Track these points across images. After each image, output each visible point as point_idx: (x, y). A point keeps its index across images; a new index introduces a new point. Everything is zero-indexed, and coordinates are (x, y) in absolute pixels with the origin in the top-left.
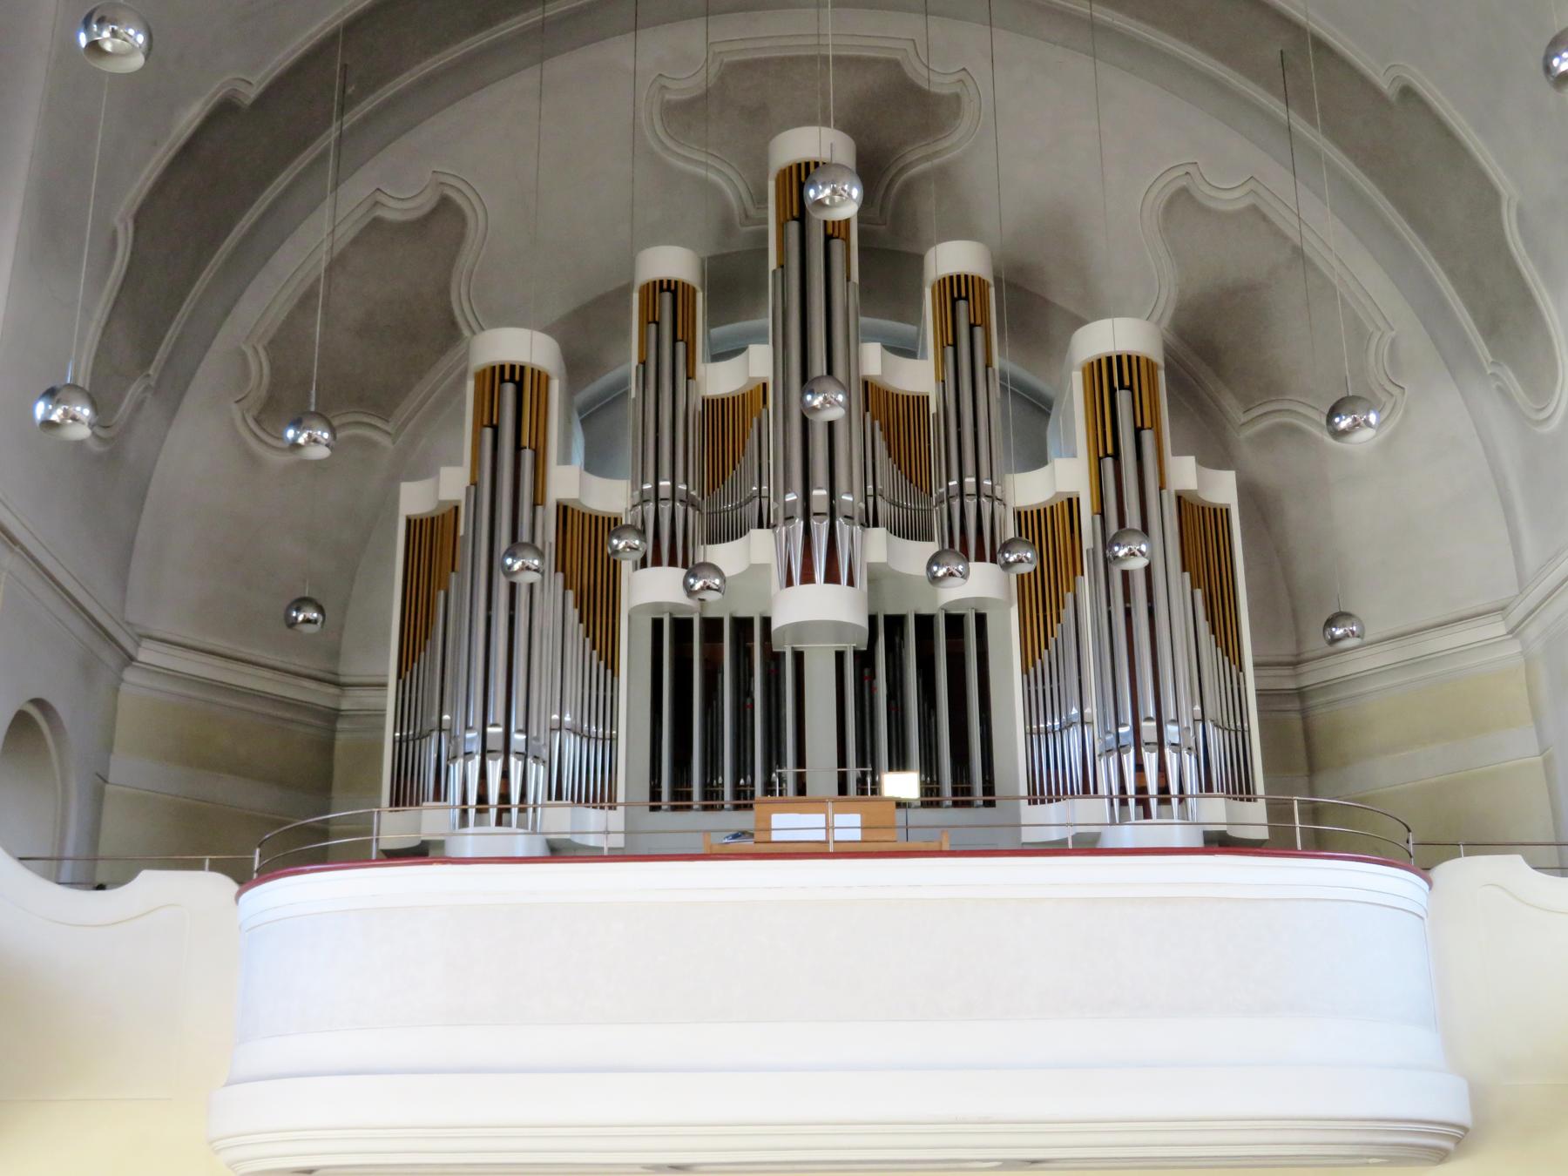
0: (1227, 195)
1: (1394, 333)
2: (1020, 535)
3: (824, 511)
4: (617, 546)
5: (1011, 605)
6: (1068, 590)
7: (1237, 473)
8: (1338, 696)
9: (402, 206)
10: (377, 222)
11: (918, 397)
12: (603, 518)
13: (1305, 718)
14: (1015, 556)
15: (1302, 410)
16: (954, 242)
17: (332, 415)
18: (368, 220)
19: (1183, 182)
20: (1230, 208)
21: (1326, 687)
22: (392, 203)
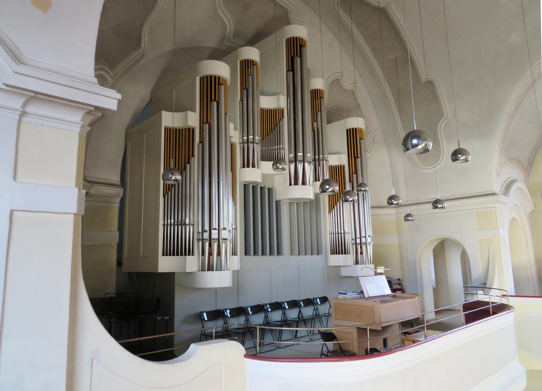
0: (348, 85)
1: (375, 133)
2: (330, 178)
6: (338, 201)
11: (267, 110)
14: (364, 189)
16: (225, 64)
17: (423, 78)
19: (339, 77)
20: (347, 88)
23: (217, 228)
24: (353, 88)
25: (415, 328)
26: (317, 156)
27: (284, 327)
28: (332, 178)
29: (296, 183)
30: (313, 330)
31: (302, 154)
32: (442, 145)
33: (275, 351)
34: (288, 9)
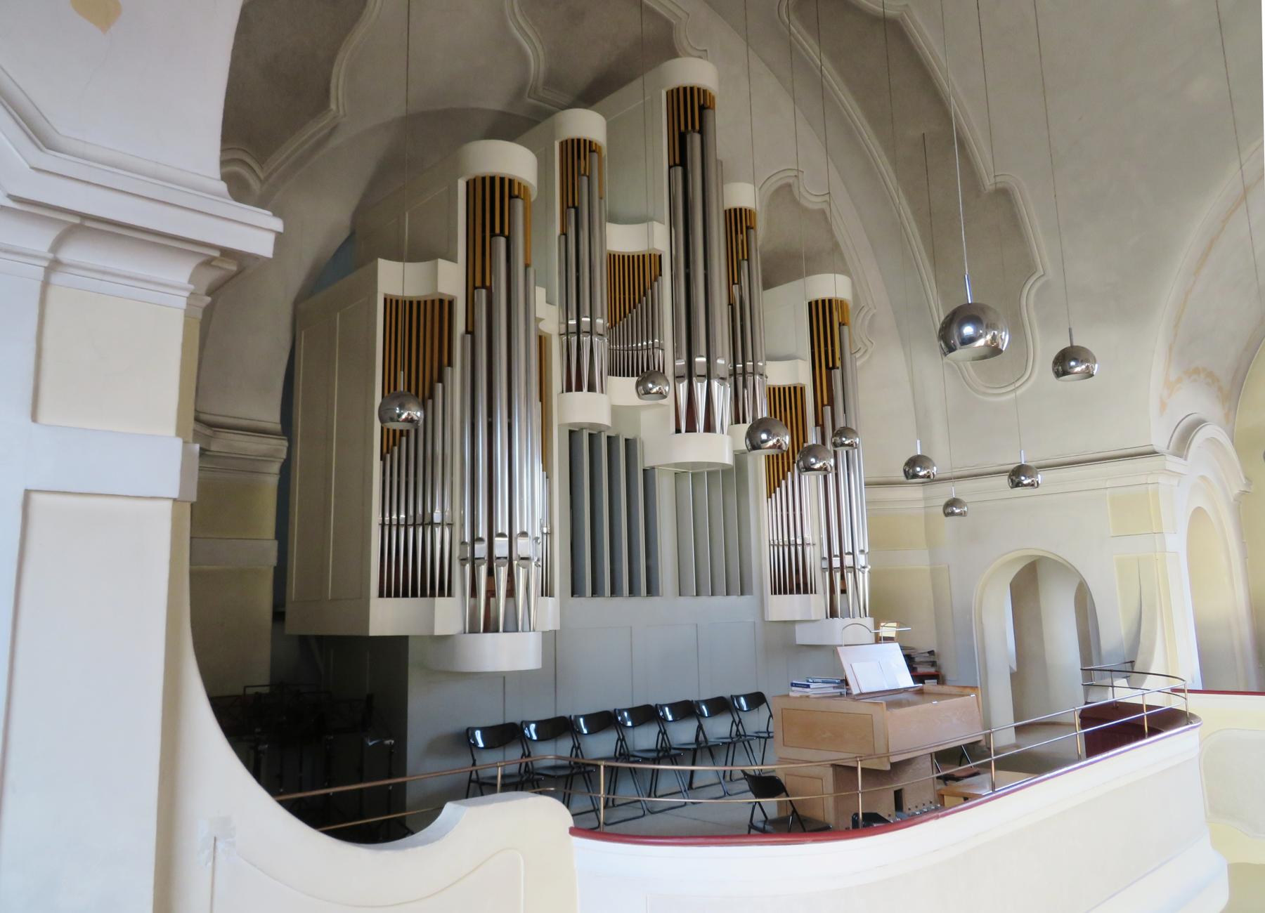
0: (811, 198)
1: (875, 311)
4: (651, 389)
6: (789, 470)
7: (268, 259)
11: (623, 257)
12: (619, 256)
14: (850, 441)
16: (526, 149)
19: (791, 181)
20: (810, 206)
23: (507, 533)
24: (824, 206)
25: (969, 765)
26: (739, 364)
27: (663, 765)
28: (776, 417)
29: (691, 428)
30: (731, 771)
31: (704, 359)
32: (1032, 337)
33: (643, 819)
34: (673, 21)
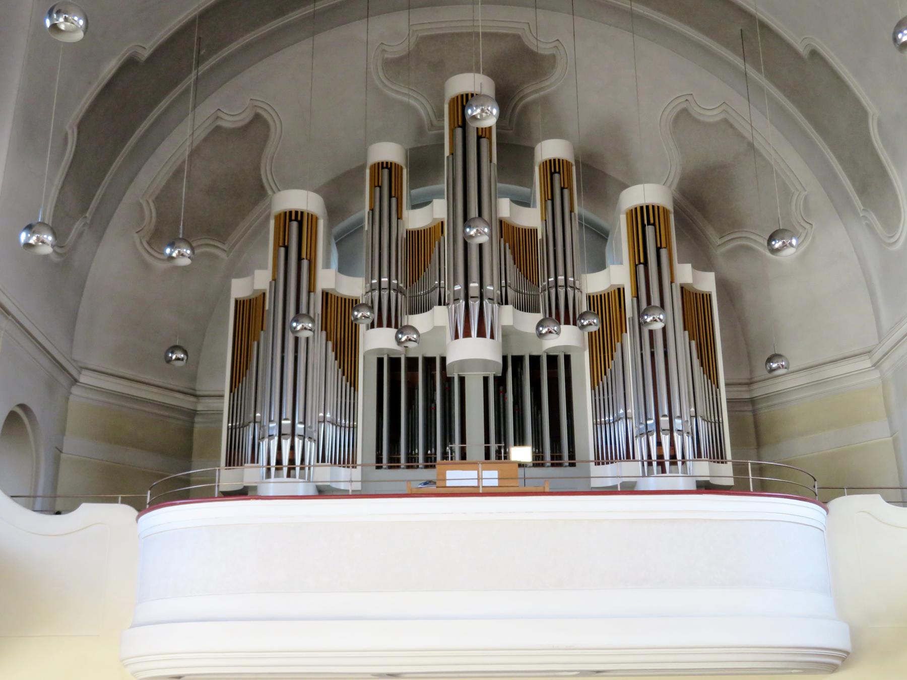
0: (710, 113)
1: (806, 193)
3: (477, 296)
5: (585, 350)
6: (618, 341)
8: (774, 402)
9: (233, 119)
10: (218, 129)
11: (531, 230)
13: (755, 415)
15: (753, 237)
16: (552, 140)
18: (213, 127)
19: (684, 106)
20: (711, 120)
21: (767, 397)
22: (227, 118)
26: (385, 278)
28: (594, 310)
31: (386, 279)
